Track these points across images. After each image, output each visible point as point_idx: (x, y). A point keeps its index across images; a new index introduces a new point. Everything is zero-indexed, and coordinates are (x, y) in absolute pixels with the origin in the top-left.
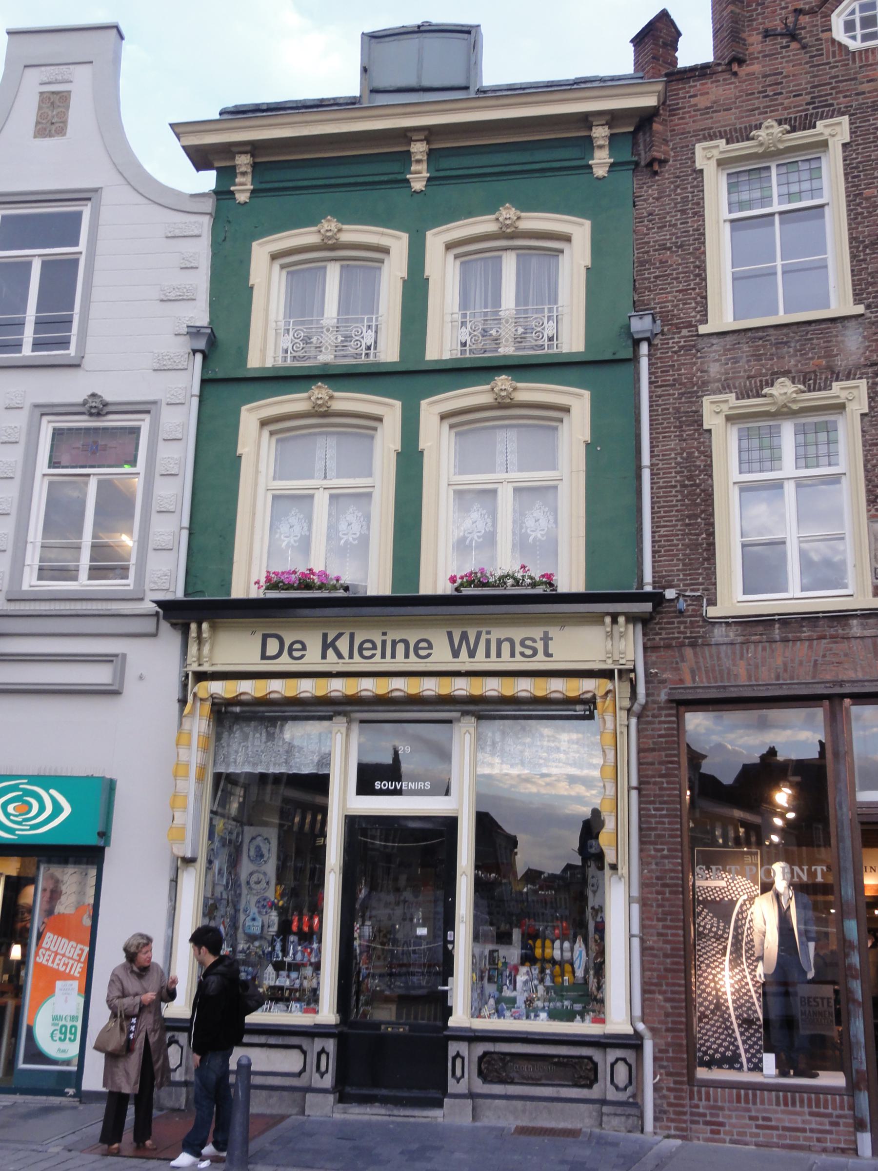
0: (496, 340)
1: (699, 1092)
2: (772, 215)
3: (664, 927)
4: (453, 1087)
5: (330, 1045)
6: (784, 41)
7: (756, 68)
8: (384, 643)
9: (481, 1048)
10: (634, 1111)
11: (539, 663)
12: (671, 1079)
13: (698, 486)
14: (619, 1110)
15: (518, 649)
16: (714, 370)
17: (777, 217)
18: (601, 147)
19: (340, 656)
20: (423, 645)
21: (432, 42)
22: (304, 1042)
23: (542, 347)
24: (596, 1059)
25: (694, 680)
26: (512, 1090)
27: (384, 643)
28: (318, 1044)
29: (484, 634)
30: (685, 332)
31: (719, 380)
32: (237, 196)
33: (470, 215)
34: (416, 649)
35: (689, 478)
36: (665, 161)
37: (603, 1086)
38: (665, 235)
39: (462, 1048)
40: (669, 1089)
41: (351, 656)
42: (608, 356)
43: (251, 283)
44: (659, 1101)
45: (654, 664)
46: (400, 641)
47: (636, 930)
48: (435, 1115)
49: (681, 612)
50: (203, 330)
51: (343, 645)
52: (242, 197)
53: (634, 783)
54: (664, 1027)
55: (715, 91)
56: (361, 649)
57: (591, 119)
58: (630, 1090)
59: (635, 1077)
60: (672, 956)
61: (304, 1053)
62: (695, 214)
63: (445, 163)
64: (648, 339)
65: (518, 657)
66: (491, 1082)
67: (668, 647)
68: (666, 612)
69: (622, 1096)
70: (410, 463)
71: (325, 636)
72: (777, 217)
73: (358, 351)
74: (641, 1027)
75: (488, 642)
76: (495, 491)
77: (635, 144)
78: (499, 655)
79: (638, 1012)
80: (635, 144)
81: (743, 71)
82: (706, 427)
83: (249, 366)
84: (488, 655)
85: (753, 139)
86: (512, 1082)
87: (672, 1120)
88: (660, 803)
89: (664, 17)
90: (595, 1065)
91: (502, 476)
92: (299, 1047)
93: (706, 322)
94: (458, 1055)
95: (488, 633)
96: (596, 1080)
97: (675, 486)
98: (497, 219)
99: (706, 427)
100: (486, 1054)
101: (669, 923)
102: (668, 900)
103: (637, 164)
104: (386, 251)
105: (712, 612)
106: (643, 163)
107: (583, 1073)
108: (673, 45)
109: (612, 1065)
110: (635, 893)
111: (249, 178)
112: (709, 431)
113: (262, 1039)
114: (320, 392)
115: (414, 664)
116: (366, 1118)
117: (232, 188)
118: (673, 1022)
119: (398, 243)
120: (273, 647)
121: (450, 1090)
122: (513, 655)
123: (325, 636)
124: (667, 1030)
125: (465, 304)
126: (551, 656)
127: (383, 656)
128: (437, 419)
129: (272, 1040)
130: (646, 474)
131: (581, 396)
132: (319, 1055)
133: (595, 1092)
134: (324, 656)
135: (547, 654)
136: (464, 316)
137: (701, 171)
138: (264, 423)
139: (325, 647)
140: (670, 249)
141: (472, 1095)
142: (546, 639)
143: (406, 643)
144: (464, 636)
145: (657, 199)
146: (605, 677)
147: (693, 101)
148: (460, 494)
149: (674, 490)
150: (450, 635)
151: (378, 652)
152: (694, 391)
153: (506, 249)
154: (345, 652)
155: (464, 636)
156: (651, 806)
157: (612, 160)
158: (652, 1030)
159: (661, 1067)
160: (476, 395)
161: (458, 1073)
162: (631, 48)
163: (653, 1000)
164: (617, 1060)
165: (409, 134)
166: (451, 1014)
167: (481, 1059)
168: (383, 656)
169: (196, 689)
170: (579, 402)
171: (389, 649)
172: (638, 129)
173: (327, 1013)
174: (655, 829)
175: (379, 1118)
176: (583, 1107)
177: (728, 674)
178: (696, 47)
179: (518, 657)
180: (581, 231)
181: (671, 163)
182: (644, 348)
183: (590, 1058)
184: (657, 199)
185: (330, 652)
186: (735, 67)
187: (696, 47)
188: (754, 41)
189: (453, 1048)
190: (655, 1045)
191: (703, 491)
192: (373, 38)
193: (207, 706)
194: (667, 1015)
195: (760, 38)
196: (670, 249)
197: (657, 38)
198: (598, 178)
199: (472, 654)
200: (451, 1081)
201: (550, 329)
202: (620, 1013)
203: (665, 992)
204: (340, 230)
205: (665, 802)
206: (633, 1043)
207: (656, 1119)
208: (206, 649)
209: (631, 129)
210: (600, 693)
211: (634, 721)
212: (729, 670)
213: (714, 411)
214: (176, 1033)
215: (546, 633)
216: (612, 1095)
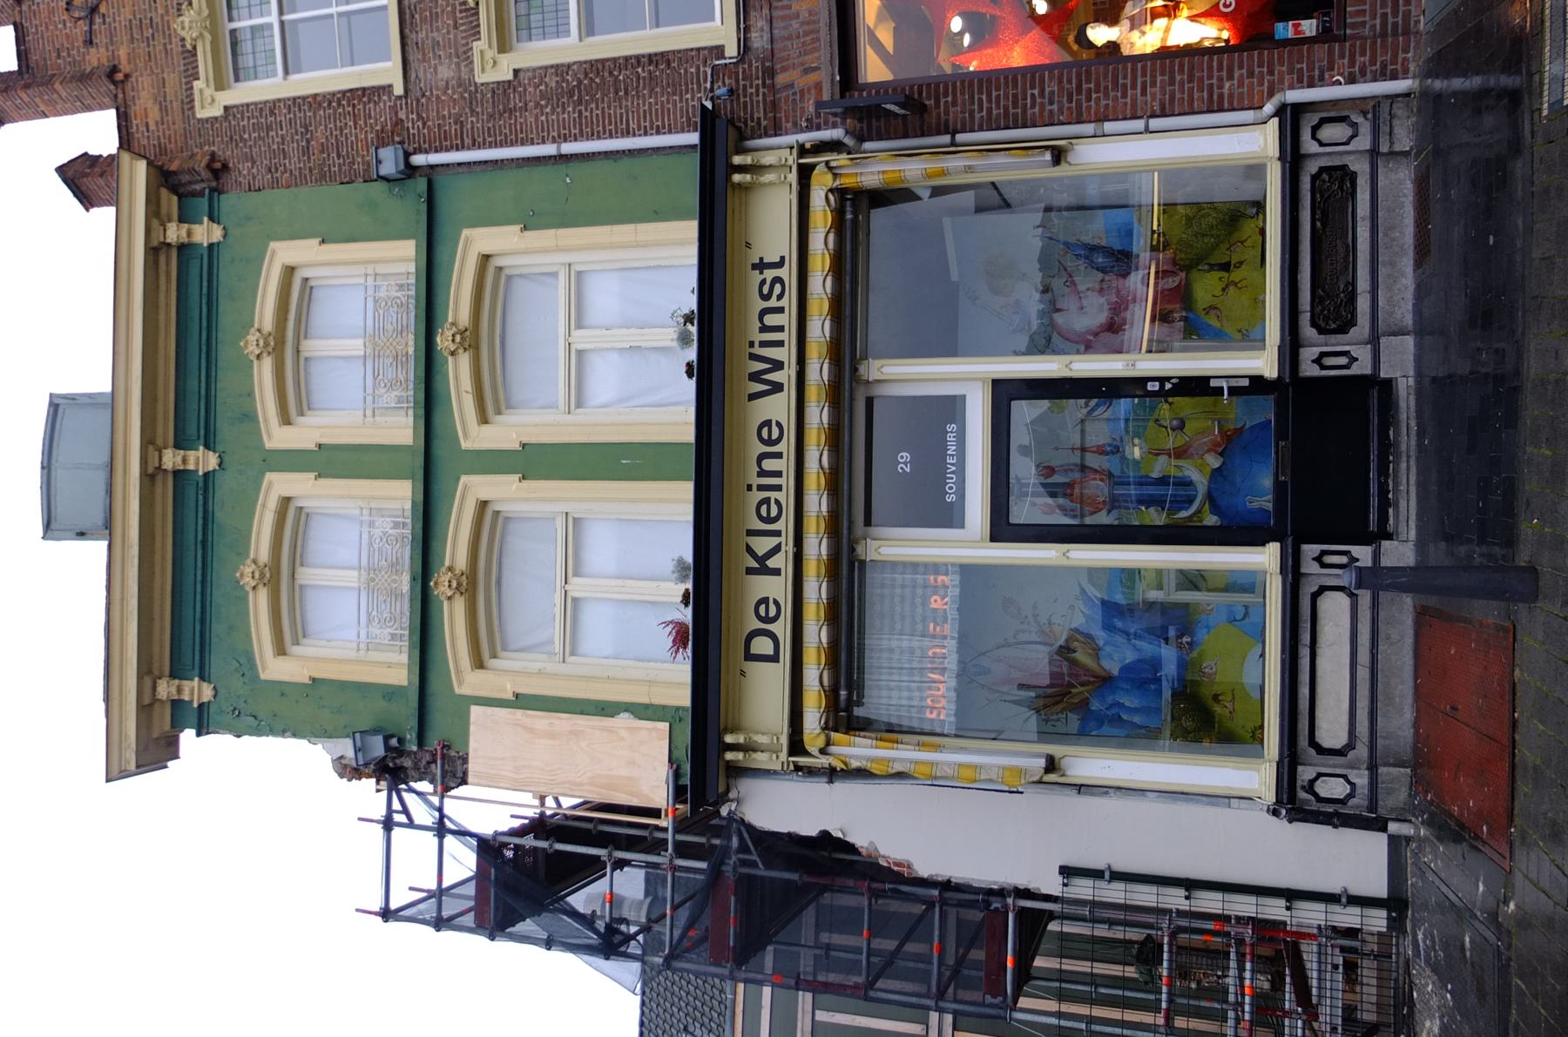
1: (1354, 26)
2: (282, 23)
3: (1134, 87)
4: (1362, 367)
5: (1311, 550)
6: (98, 20)
7: (123, 53)
8: (761, 488)
9: (1307, 331)
10: (1385, 107)
11: (789, 274)
12: (1338, 62)
13: (580, 82)
14: (1385, 129)
15: (773, 303)
16: (445, 72)
17: (285, 18)
18: (189, 234)
21: (60, 456)
22: (1308, 589)
24: (1314, 170)
25: (817, 68)
26: (1363, 284)
27: (761, 488)
28: (1309, 567)
29: (753, 351)
30: (402, 115)
31: (458, 65)
32: (205, 700)
35: (571, 95)
36: (213, 154)
37: (1352, 157)
38: (292, 148)
39: (1308, 354)
40: (1352, 63)
41: (777, 533)
42: (424, 207)
43: (307, 681)
44: (1369, 76)
45: (795, 124)
46: (759, 465)
47: (1139, 124)
48: (1405, 388)
49: (731, 92)
50: (359, 744)
51: (762, 545)
53: (946, 139)
54: (1267, 78)
55: (144, 102)
57: (155, 243)
58: (1359, 119)
59: (1335, 113)
60: (1172, 72)
61: (1323, 589)
62: (272, 113)
63: (192, 429)
64: (407, 155)
65: (784, 303)
66: (1353, 312)
67: (774, 106)
68: (732, 112)
69: (1365, 128)
70: (537, 461)
71: (750, 571)
72: (285, 18)
74: (1269, 108)
75: (763, 344)
76: (580, 353)
77: (194, 194)
79: (1248, 116)
80: (194, 194)
81: (125, 67)
82: (510, 76)
83: (405, 683)
84: (780, 344)
85: (195, 48)
86: (1354, 284)
87: (1395, 56)
88: (973, 103)
89: (62, 170)
90: (1322, 170)
92: (1315, 597)
93: (390, 86)
94: (1318, 361)
95: (752, 344)
96: (1344, 168)
97: (580, 112)
98: (449, 598)
99: (510, 76)
100: (1314, 324)
101: (1129, 82)
102: (1097, 85)
103: (212, 190)
105: (731, 51)
106: (214, 184)
107: (1338, 181)
108: (95, 160)
109: (1321, 144)
110: (1089, 128)
111: (186, 683)
112: (516, 72)
113: (1305, 653)
114: (442, 585)
116: (1413, 489)
117: (195, 705)
118: (1261, 65)
120: (762, 646)
121: (1368, 371)
123: (750, 571)
124: (1271, 72)
126: (783, 258)
127: (778, 488)
128: (485, 427)
129: (1306, 637)
130: (569, 148)
131: (467, 239)
132: (1324, 565)
133: (1361, 167)
134: (777, 572)
137: (226, 108)
138: (479, 664)
139: (764, 570)
140: (308, 141)
141: (1374, 340)
142: (761, 266)
144: (755, 377)
145: (254, 162)
146: (809, 178)
147: (152, 127)
149: (585, 114)
151: (773, 495)
152: (472, 93)
154: (772, 542)
155: (755, 377)
156: (977, 116)
157: (206, 219)
158: (1271, 95)
159: (1322, 78)
160: (458, 373)
161: (1343, 361)
162: (94, 211)
163: (1231, 96)
164: (1314, 137)
165: (150, 470)
166: (1260, 378)
167: (1321, 331)
168: (778, 488)
169: (814, 750)
170: (477, 241)
172: (174, 189)
173: (1265, 558)
174: (1006, 109)
175: (1413, 470)
176: (1382, 181)
177: (808, 23)
178: (96, 132)
179: (784, 303)
180: (284, 253)
181: (215, 149)
182: (419, 160)
183: (1314, 178)
184: (254, 162)
185: (771, 563)
186: (120, 76)
187: (96, 132)
188: (96, 57)
189: (1309, 370)
190: (1292, 87)
191: (586, 75)
192: (50, 528)
193: (835, 736)
194: (1251, 74)
195: (93, 50)
196: (308, 141)
197: (85, 179)
198: (225, 237)
199: (778, 365)
200: (1355, 370)
202: (1251, 141)
203: (1220, 79)
204: (255, 561)
205: (972, 97)
206: (1291, 117)
207: (1394, 77)
208: (761, 739)
209: (175, 198)
210: (828, 181)
211: (868, 145)
212: (803, 23)
213: (492, 68)
214: (1299, 783)
215: (754, 267)
216: (1363, 142)
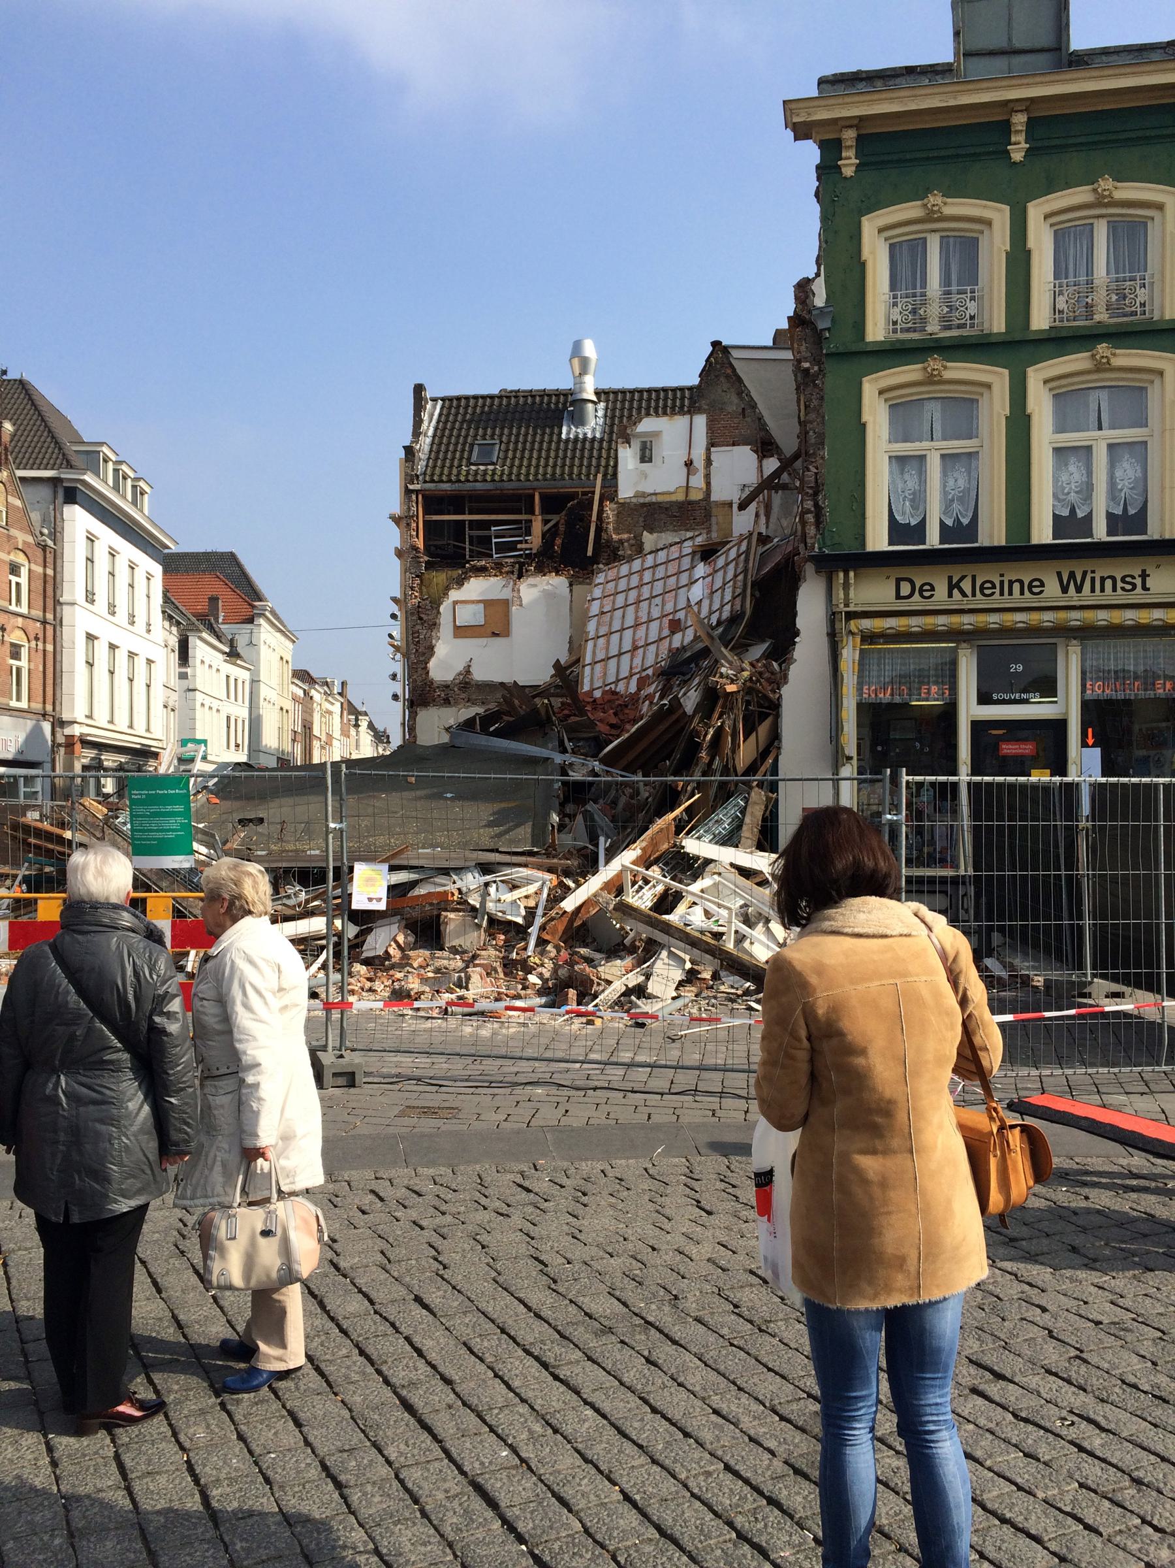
0: (924, 320)
8: (1002, 583)
11: (1138, 596)
15: (1119, 584)
19: (964, 594)
20: (1037, 583)
23: (1134, 313)
27: (1002, 583)
32: (843, 170)
33: (1068, 186)
34: (1030, 587)
41: (974, 595)
51: (966, 585)
52: (848, 172)
56: (982, 588)
65: (1119, 592)
73: (963, 321)
75: (1093, 580)
78: (1103, 590)
84: (1093, 590)
91: (926, 444)
104: (988, 223)
115: (1028, 599)
119: (1000, 215)
120: (905, 589)
122: (1114, 589)
123: (950, 578)
125: (893, 286)
127: (1002, 594)
134: (950, 595)
135: (1145, 588)
136: (895, 297)
142: (1144, 576)
143: (1021, 582)
148: (1057, 450)
150: (1059, 574)
151: (997, 591)
153: (1098, 217)
154: (968, 591)
155: (1072, 575)
168: (1002, 594)
171: (1006, 588)
173: (965, 869)
179: (1119, 592)
185: (955, 591)
199: (1079, 589)
201: (972, 308)
